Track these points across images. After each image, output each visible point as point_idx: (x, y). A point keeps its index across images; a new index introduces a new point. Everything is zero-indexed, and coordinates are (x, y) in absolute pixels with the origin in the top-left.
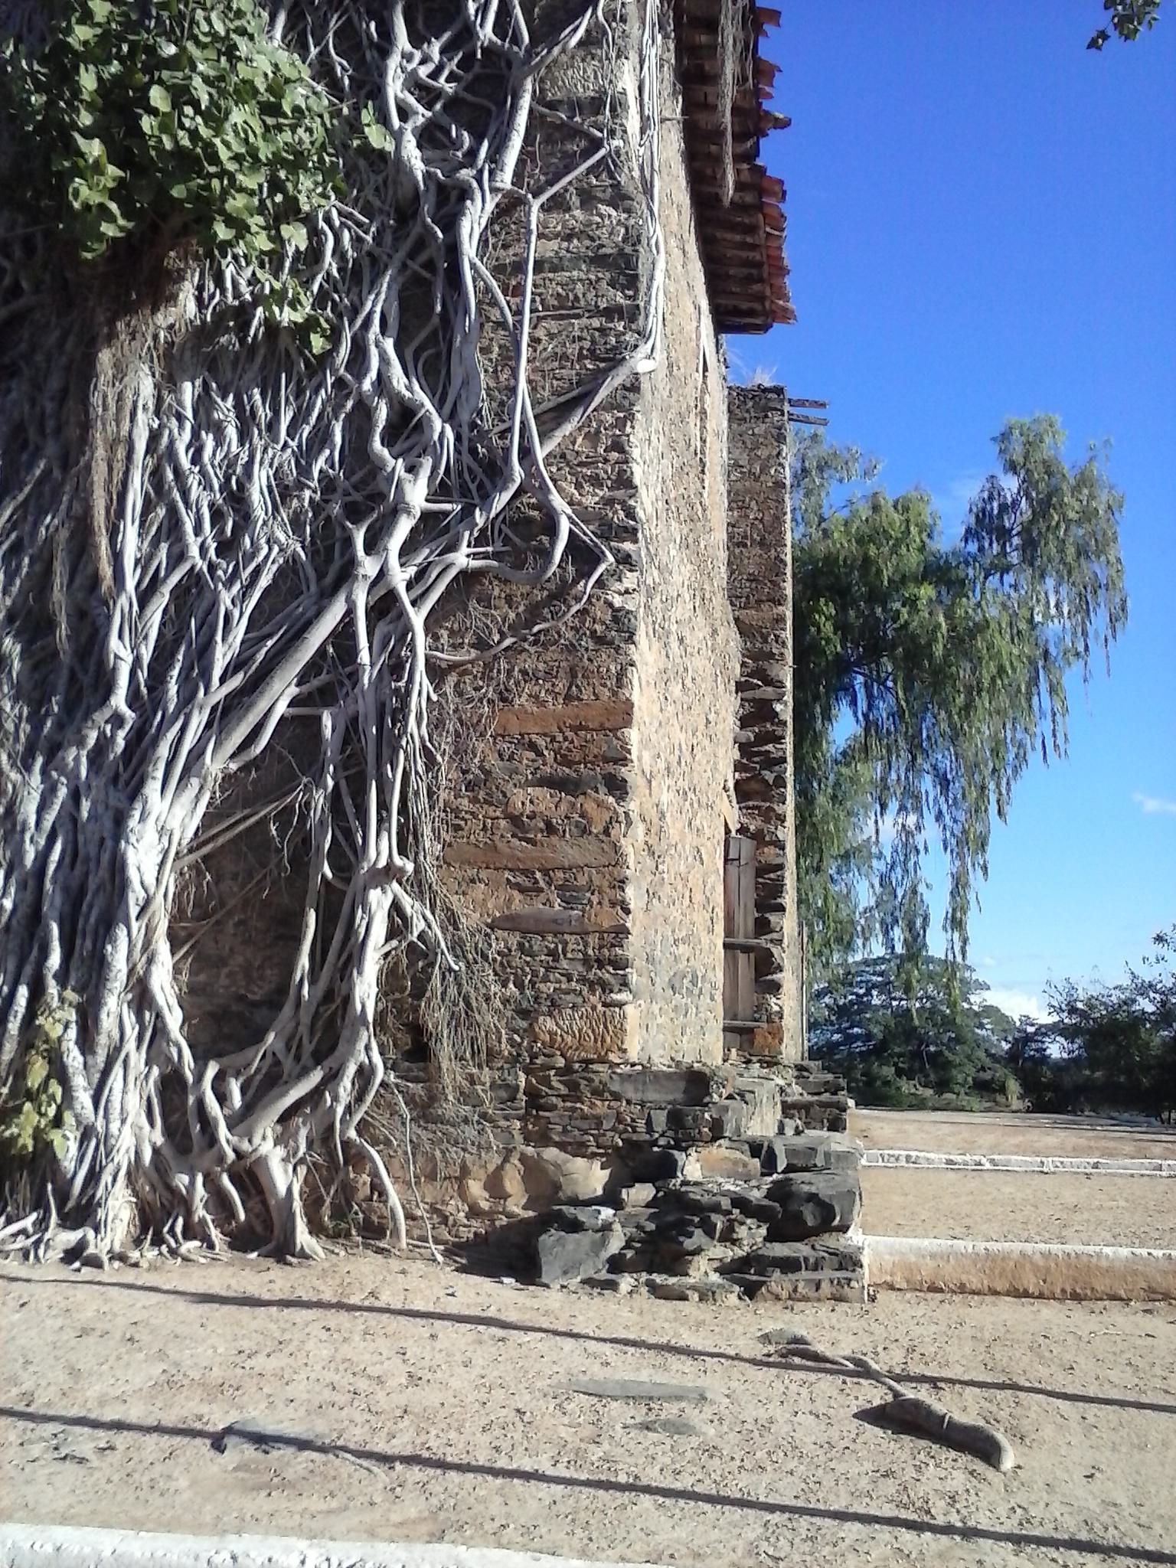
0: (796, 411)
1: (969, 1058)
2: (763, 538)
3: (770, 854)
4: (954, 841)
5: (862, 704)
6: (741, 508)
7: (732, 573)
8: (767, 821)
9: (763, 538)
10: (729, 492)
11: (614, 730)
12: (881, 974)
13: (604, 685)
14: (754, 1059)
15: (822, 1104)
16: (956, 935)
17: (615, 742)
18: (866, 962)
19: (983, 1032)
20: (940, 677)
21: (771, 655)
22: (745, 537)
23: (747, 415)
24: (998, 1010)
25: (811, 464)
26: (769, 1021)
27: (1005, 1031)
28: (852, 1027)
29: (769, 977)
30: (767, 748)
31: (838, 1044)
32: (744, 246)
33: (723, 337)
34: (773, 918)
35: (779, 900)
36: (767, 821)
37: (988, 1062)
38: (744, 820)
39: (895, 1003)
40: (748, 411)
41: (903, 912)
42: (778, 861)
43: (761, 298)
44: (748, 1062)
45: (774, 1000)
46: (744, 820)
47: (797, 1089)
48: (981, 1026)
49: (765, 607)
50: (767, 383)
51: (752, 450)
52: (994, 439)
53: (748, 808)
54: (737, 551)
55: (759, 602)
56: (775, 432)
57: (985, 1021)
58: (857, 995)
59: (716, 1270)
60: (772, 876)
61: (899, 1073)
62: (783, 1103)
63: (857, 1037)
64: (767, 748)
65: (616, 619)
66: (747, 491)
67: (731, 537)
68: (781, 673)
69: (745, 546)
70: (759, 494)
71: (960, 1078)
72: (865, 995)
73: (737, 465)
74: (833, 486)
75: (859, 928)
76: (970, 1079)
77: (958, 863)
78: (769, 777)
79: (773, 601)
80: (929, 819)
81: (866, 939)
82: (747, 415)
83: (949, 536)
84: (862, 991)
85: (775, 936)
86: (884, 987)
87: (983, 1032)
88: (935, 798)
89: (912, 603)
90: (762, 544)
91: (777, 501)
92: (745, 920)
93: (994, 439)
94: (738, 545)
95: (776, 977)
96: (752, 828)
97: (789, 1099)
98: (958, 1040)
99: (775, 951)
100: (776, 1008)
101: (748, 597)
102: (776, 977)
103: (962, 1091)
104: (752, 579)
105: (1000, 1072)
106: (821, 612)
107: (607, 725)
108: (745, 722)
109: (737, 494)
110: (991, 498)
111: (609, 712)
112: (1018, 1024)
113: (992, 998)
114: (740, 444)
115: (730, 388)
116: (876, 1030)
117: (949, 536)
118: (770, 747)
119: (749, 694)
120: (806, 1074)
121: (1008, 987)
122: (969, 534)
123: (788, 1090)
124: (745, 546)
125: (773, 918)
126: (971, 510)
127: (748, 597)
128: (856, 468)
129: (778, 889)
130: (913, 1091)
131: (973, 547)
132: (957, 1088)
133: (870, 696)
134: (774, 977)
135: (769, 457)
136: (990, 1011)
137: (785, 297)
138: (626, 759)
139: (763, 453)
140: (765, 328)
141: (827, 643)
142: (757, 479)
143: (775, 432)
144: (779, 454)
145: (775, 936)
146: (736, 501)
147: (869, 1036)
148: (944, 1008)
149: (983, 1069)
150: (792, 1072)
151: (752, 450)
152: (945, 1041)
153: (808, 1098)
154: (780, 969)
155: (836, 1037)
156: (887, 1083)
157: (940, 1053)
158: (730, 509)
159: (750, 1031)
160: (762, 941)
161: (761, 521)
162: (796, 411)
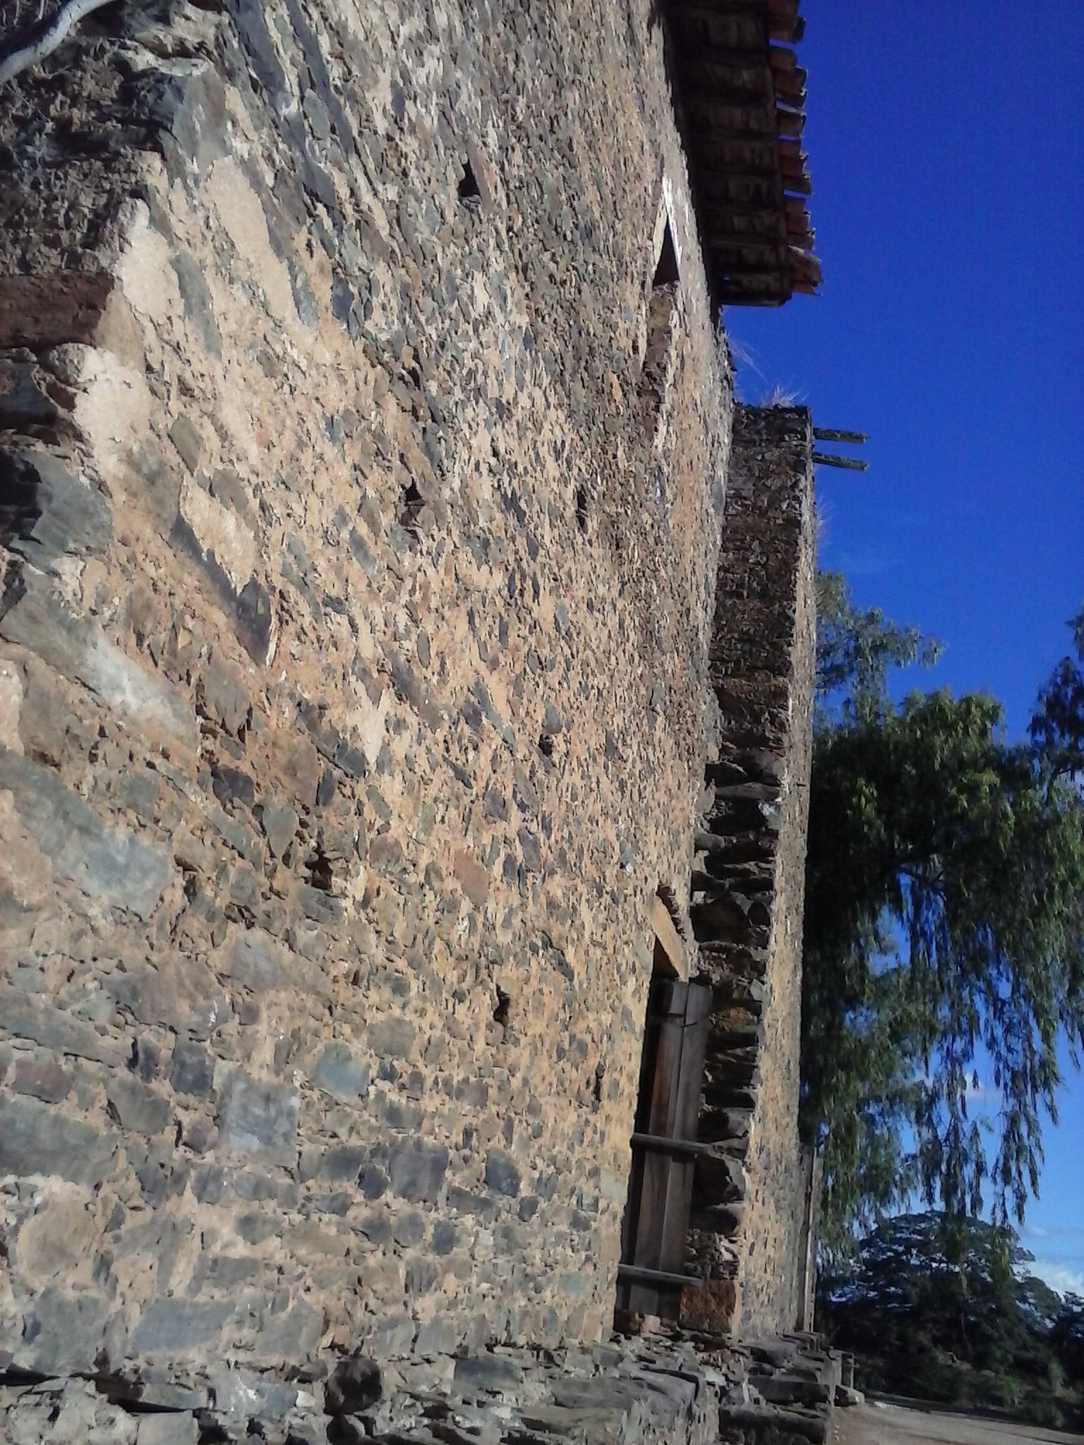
0: (826, 448)
1: (1010, 1333)
2: (765, 589)
3: (737, 1018)
4: (1008, 1075)
5: (909, 909)
6: (738, 549)
7: (719, 629)
8: (738, 970)
9: (765, 589)
10: (724, 529)
11: (42, 348)
12: (919, 1233)
13: (53, 243)
14: (687, 1334)
15: (783, 1424)
16: (1008, 1192)
17: (36, 373)
18: (906, 1218)
19: (1026, 1307)
20: (1003, 879)
21: (763, 741)
22: (741, 585)
23: (756, 437)
24: (1041, 1283)
25: (866, 642)
26: (716, 1275)
27: (1048, 1307)
28: (889, 1286)
29: (721, 1206)
30: (746, 866)
31: (872, 1302)
32: (747, 133)
33: (725, 310)
34: (734, 1115)
35: (745, 1090)
36: (738, 970)
37: (1030, 1341)
38: (705, 966)
39: (934, 1265)
40: (758, 432)
41: (944, 1161)
42: (749, 1029)
43: (772, 239)
44: (676, 1337)
45: (725, 1243)
46: (705, 966)
47: (748, 1391)
48: (1024, 1300)
49: (760, 676)
50: (787, 402)
51: (759, 478)
52: (1070, 623)
53: (711, 949)
54: (729, 602)
55: (753, 669)
56: (791, 458)
57: (1028, 1294)
58: (895, 1251)
59: (854, 1403)
60: (739, 1052)
61: (936, 1341)
62: (723, 1415)
63: (894, 1297)
64: (746, 866)
65: (128, 94)
66: (749, 528)
67: (721, 584)
68: (775, 766)
69: (740, 596)
70: (764, 534)
71: (998, 1354)
72: (904, 1253)
73: (738, 496)
74: (888, 670)
75: (897, 1177)
76: (1010, 1357)
77: (1012, 1101)
78: (743, 902)
79: (772, 669)
80: (980, 1046)
81: (904, 1191)
82: (756, 437)
83: (1012, 734)
84: (901, 1249)
85: (735, 1143)
86: (924, 1247)
87: (1026, 1307)
88: (987, 1020)
89: (972, 790)
90: (763, 595)
91: (786, 542)
92: (683, 1109)
93: (1070, 623)
94: (730, 594)
95: (732, 1207)
96: (716, 978)
97: (733, 1409)
98: (1000, 1312)
99: (732, 1165)
100: (727, 1256)
101: (737, 662)
102: (732, 1207)
103: (1002, 1369)
104: (746, 638)
105: (1043, 1353)
106: (860, 793)
107: (30, 333)
108: (716, 826)
109: (735, 531)
110: (1066, 681)
111: (45, 302)
112: (1063, 1300)
113: (1037, 1270)
114: (744, 471)
115: (738, 404)
116: (913, 1292)
117: (1012, 734)
118: (751, 866)
119: (728, 791)
120: (767, 1366)
121: (1054, 1260)
122: (1037, 725)
123: (734, 1394)
124: (740, 596)
125: (734, 1115)
126: (1040, 697)
127: (737, 662)
128: (915, 651)
129: (745, 1071)
130: (950, 1362)
131: (1041, 738)
132: (996, 1365)
133: (917, 906)
134: (729, 1206)
135: (783, 488)
136: (1034, 1284)
137: (801, 238)
138: (51, 418)
139: (774, 483)
140: (782, 297)
141: (871, 827)
142: (763, 514)
143: (791, 458)
144: (795, 485)
145: (735, 1143)
146: (733, 539)
147: (904, 1298)
148: (985, 1275)
149: (1025, 1347)
150: (746, 1362)
151: (759, 478)
152: (985, 1311)
153: (767, 1409)
154: (737, 1195)
155: (872, 1294)
156: (922, 1350)
157: (976, 1325)
158: (724, 549)
159: (676, 1288)
160: (710, 1150)
161: (764, 566)
162: (826, 448)
